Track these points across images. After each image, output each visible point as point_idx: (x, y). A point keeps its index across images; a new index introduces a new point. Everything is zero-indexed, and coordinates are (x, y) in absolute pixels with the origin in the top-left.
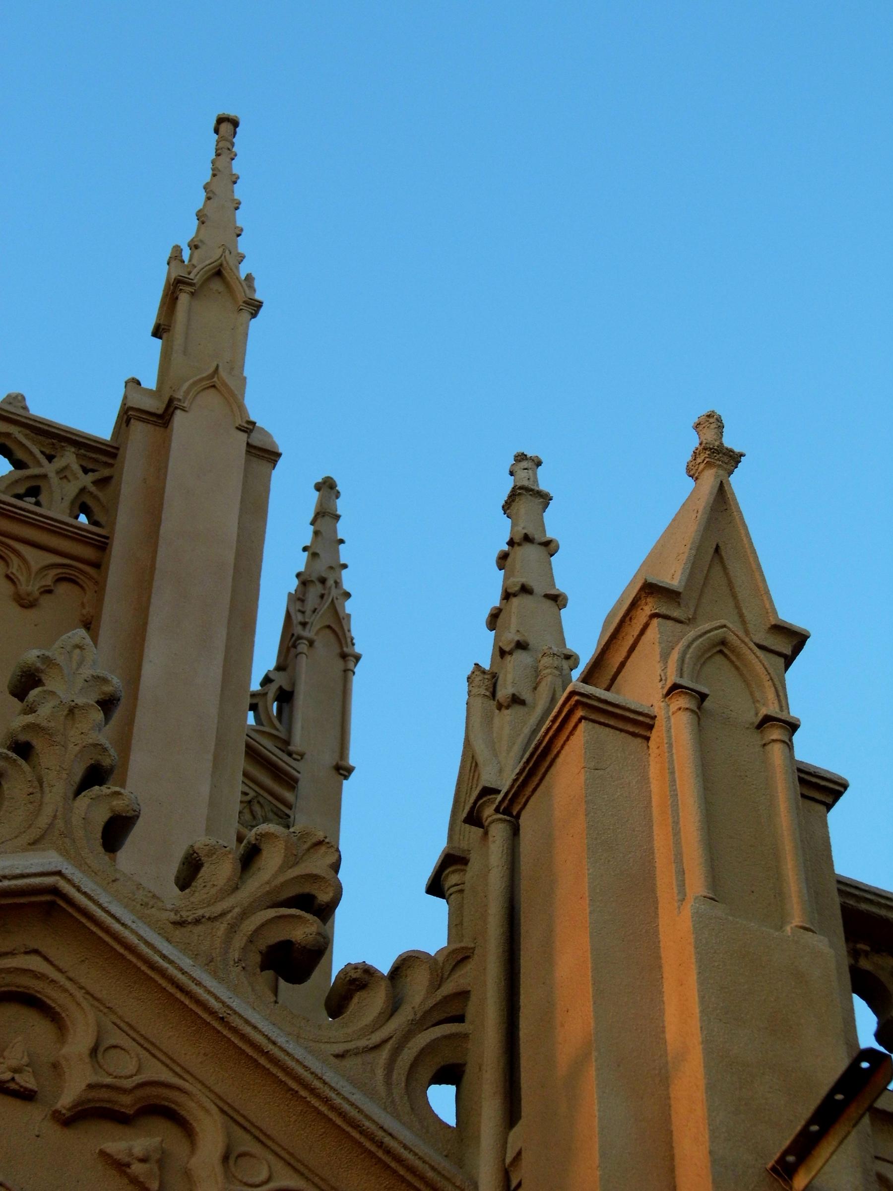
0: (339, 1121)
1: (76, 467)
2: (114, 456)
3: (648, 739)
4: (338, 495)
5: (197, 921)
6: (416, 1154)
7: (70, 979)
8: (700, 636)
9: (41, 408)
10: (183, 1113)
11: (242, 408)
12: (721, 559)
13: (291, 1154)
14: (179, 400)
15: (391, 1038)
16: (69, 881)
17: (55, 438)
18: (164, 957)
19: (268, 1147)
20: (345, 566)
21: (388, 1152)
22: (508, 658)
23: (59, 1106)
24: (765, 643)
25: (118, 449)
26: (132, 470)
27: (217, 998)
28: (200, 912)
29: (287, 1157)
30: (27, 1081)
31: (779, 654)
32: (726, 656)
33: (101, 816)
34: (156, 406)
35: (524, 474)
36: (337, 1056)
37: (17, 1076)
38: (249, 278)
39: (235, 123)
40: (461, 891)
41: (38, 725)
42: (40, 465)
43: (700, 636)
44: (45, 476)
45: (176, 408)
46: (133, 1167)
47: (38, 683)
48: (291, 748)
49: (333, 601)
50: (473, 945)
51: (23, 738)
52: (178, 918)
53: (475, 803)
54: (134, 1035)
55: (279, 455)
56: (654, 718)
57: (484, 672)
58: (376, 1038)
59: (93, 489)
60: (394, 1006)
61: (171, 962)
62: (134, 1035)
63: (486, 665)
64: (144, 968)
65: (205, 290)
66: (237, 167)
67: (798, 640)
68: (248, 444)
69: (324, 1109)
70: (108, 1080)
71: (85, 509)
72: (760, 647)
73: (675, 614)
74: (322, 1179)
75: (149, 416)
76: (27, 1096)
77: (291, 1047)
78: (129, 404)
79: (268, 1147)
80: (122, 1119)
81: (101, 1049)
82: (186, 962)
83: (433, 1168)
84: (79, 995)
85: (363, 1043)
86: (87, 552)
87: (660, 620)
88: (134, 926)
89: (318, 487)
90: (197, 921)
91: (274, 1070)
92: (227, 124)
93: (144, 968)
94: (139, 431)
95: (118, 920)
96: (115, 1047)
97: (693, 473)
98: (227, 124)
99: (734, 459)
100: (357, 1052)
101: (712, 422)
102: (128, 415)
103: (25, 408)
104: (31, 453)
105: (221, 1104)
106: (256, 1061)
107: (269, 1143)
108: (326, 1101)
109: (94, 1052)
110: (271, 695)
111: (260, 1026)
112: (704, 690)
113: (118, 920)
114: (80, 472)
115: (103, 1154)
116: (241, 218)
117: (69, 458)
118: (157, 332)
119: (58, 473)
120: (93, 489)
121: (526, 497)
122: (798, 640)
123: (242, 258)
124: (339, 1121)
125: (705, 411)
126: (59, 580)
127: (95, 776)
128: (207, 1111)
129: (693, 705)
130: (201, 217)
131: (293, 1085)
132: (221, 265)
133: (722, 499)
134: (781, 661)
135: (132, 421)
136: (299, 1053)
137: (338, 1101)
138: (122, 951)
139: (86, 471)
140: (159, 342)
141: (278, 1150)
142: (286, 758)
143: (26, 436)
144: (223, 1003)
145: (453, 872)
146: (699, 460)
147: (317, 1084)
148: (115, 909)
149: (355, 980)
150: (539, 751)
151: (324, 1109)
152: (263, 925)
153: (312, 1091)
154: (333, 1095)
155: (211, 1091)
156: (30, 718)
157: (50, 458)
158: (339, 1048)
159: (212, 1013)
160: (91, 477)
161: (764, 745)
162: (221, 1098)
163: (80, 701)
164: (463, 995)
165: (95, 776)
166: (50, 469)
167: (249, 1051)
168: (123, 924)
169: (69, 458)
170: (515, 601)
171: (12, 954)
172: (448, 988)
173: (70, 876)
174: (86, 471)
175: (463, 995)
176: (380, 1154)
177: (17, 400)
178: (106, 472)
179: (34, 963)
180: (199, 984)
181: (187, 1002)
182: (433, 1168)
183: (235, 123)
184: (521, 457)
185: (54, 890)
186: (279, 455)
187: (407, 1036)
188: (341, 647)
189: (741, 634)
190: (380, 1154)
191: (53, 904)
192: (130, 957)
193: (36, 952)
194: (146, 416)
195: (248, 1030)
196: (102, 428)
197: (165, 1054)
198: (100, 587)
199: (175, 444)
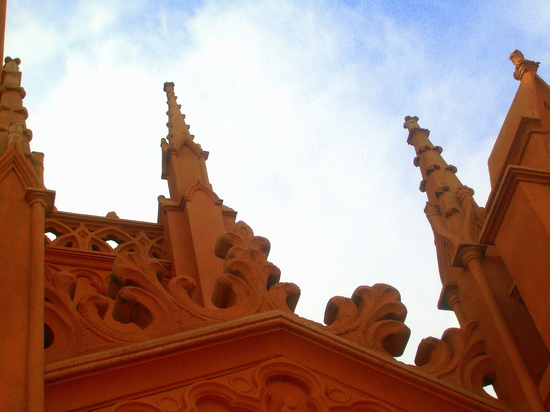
1: (146, 238)
14: (187, 197)
15: (457, 366)
16: (286, 319)
18: (344, 344)
25: (163, 226)
27: (376, 358)
28: (347, 328)
35: (412, 125)
41: (240, 261)
42: (130, 240)
44: (134, 244)
45: (186, 201)
47: (231, 246)
50: (477, 320)
51: (234, 268)
52: (338, 332)
55: (236, 213)
58: (450, 367)
59: (157, 245)
60: (452, 355)
65: (182, 156)
66: (178, 102)
68: (223, 212)
70: (339, 405)
73: (539, 130)
81: (329, 392)
82: (355, 345)
88: (325, 333)
96: (335, 390)
97: (517, 77)
101: (516, 55)
108: (445, 393)
114: (149, 240)
116: (187, 121)
118: (164, 177)
120: (157, 245)
121: (416, 134)
125: (513, 50)
131: (426, 390)
132: (186, 140)
133: (539, 82)
135: (167, 212)
138: (323, 346)
139: (151, 239)
143: (120, 229)
146: (520, 69)
150: (499, 203)
152: (378, 329)
153: (437, 390)
166: (135, 241)
169: (143, 234)
171: (269, 358)
172: (472, 341)
174: (151, 239)
177: (112, 215)
178: (161, 237)
181: (362, 363)
184: (408, 118)
185: (281, 325)
186: (236, 213)
194: (173, 208)
199: (190, 216)
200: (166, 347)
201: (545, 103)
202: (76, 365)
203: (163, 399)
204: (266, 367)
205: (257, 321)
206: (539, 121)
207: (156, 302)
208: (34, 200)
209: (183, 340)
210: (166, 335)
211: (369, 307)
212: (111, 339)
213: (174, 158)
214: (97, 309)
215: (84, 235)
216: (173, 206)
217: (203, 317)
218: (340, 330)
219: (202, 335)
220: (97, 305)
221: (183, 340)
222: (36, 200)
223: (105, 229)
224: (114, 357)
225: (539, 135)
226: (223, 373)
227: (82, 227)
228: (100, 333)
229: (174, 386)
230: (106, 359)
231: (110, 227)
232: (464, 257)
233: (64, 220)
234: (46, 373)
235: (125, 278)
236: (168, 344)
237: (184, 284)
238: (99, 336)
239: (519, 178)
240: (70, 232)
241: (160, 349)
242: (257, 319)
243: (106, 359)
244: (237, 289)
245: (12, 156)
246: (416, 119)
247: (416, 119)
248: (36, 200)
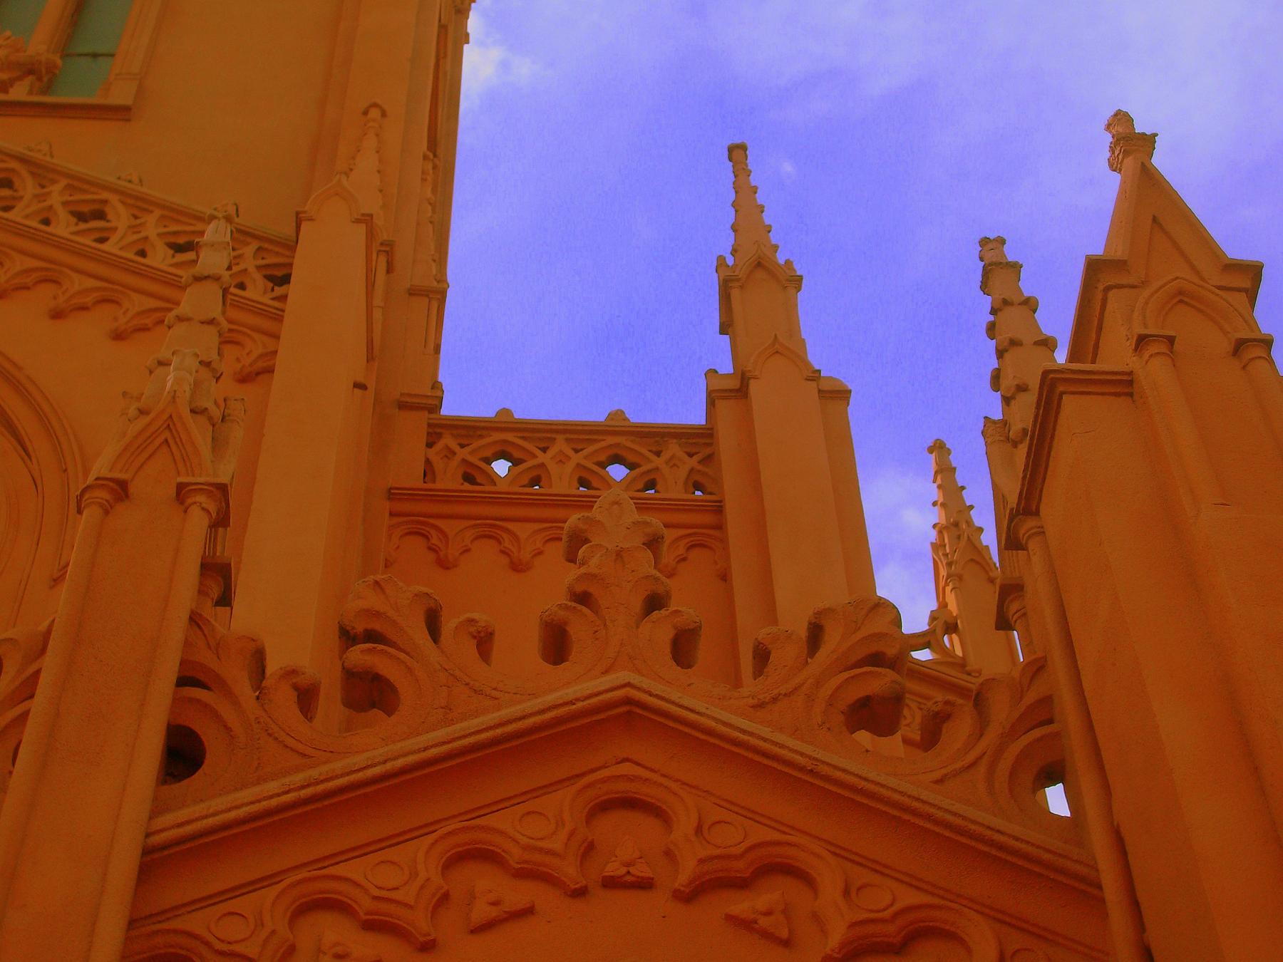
0: (947, 833)
1: (680, 454)
2: (711, 436)
3: (1131, 395)
4: (949, 451)
5: (775, 700)
6: (1028, 842)
7: (663, 776)
8: (1156, 292)
9: (639, 416)
10: (797, 864)
11: (807, 364)
12: (1160, 226)
13: (911, 876)
16: (639, 689)
17: (657, 436)
18: (744, 731)
19: (888, 875)
20: (971, 507)
21: (1001, 847)
22: (1013, 402)
23: (676, 885)
24: (1223, 284)
26: (727, 442)
27: (802, 754)
28: (776, 692)
29: (907, 879)
30: (641, 870)
31: (1239, 290)
32: (1186, 303)
33: (664, 635)
34: (735, 384)
36: (937, 782)
37: (632, 870)
38: (788, 263)
39: (743, 148)
40: (1025, 614)
42: (649, 460)
43: (1156, 292)
46: (760, 922)
47: (587, 541)
48: (968, 668)
49: (969, 538)
51: (579, 588)
52: (755, 701)
53: (1009, 528)
54: (736, 809)
55: (850, 391)
56: (1131, 373)
57: (994, 422)
58: (971, 757)
59: (700, 467)
61: (751, 734)
62: (736, 809)
63: (997, 415)
64: (727, 746)
66: (754, 180)
67: (1254, 272)
68: (819, 391)
69: (928, 825)
70: (718, 852)
71: (697, 486)
72: (1219, 288)
73: (1124, 281)
74: (947, 891)
75: (731, 393)
76: (644, 885)
77: (882, 779)
78: (711, 388)
79: (888, 875)
80: (741, 884)
81: (705, 827)
83: (1049, 851)
84: (674, 786)
85: (958, 765)
86: (709, 519)
87: (1115, 291)
88: (708, 712)
89: (931, 450)
90: (775, 700)
91: (872, 804)
92: (737, 152)
93: (727, 746)
94: (722, 406)
95: (692, 711)
98: (737, 152)
99: (1148, 141)
100: (956, 774)
101: (1121, 120)
102: (712, 400)
103: (626, 419)
104: (641, 454)
105: (833, 849)
106: (853, 800)
107: (887, 871)
108: (928, 817)
109: (699, 830)
110: (939, 631)
111: (848, 768)
112: (1172, 333)
113: (692, 711)
115: (730, 918)
117: (674, 449)
118: (723, 330)
119: (667, 463)
120: (700, 467)
122: (1254, 272)
123: (775, 248)
124: (947, 833)
126: (690, 547)
127: (654, 603)
128: (819, 856)
129: (1163, 348)
130: (734, 228)
131: (896, 813)
134: (1243, 297)
136: (892, 782)
137: (940, 814)
140: (727, 338)
141: (897, 875)
142: (969, 678)
144: (810, 757)
145: (1012, 601)
147: (915, 804)
148: (686, 701)
149: (938, 713)
151: (928, 825)
153: (914, 812)
154: (933, 811)
155: (820, 839)
156: (583, 570)
157: (658, 454)
158: (937, 775)
159: (802, 769)
160: (696, 458)
161: (1244, 367)
162: (830, 843)
163: (626, 545)
164: (1047, 701)
165: (654, 603)
167: (847, 794)
168: (698, 713)
169: (674, 449)
170: (1007, 356)
171: (604, 767)
172: (1031, 697)
173: (639, 685)
175: (1047, 701)
176: (994, 852)
178: (707, 451)
179: (626, 769)
180: (782, 746)
182: (1049, 851)
183: (743, 148)
184: (984, 242)
185: (628, 701)
186: (850, 391)
187: (1000, 750)
188: (987, 572)
189: (1196, 280)
190: (994, 852)
191: (629, 712)
192: (712, 740)
193: (627, 760)
195: (838, 774)
196: (695, 416)
197: (769, 818)
198: (724, 541)
200: (389, 766)
201: (1154, 219)
202: (214, 815)
203: (219, 919)
204: (589, 786)
205: (578, 700)
206: (1124, 262)
207: (410, 669)
208: (189, 501)
209: (426, 749)
210: (419, 734)
211: (833, 641)
212: (309, 751)
213: (735, 294)
214: (296, 693)
215: (562, 459)
216: (731, 391)
217: (494, 693)
218: (761, 697)
219: (465, 737)
220: (296, 687)
221: (426, 749)
222: (193, 499)
223: (603, 444)
224: (287, 792)
225: (1126, 290)
226: (507, 804)
227: (560, 445)
228: (289, 741)
229: (407, 837)
230: (271, 797)
231: (611, 440)
232: (1022, 532)
233: (526, 434)
234: (148, 835)
235: (360, 627)
236: (396, 758)
237: (472, 629)
238: (286, 746)
239: (1061, 389)
240: (535, 456)
241: (377, 770)
242: (579, 695)
243: (271, 797)
244: (579, 630)
245: (165, 416)
246: (1002, 241)
247: (1002, 241)
248: (193, 499)
